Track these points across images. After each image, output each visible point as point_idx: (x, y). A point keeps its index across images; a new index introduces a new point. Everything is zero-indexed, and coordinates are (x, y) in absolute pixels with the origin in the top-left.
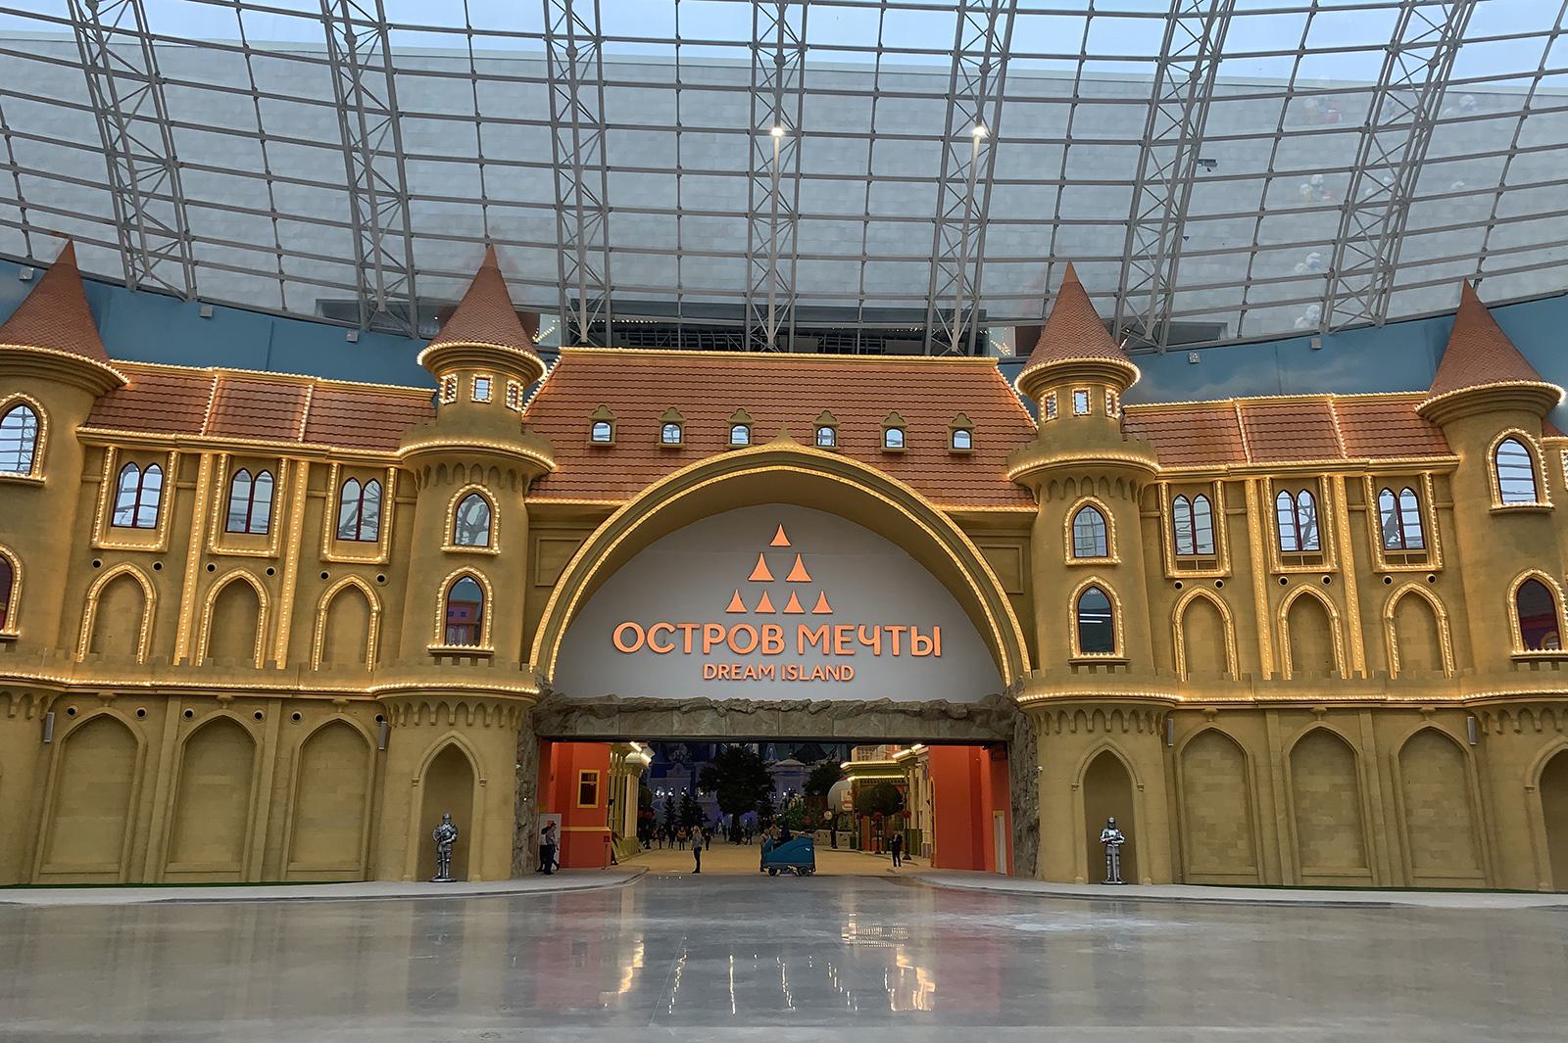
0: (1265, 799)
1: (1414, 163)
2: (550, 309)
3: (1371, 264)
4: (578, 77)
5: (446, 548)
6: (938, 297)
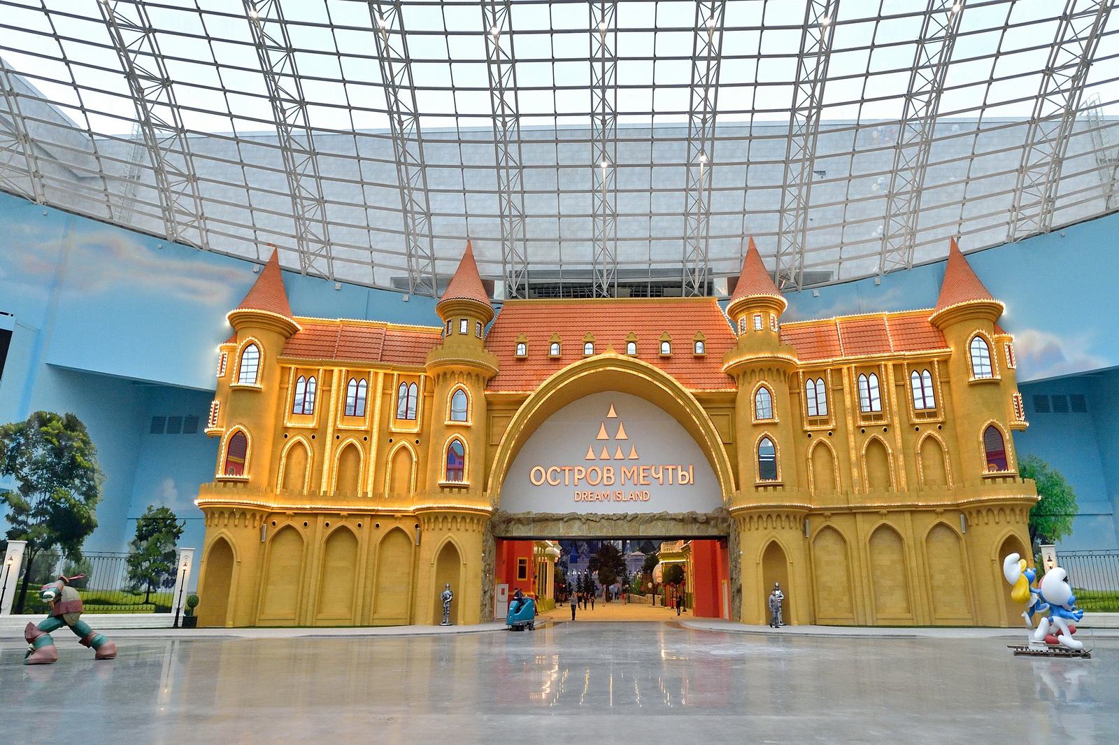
0: (857, 571)
2: (500, 278)
3: (903, 231)
4: (508, 139)
5: (446, 423)
6: (687, 261)
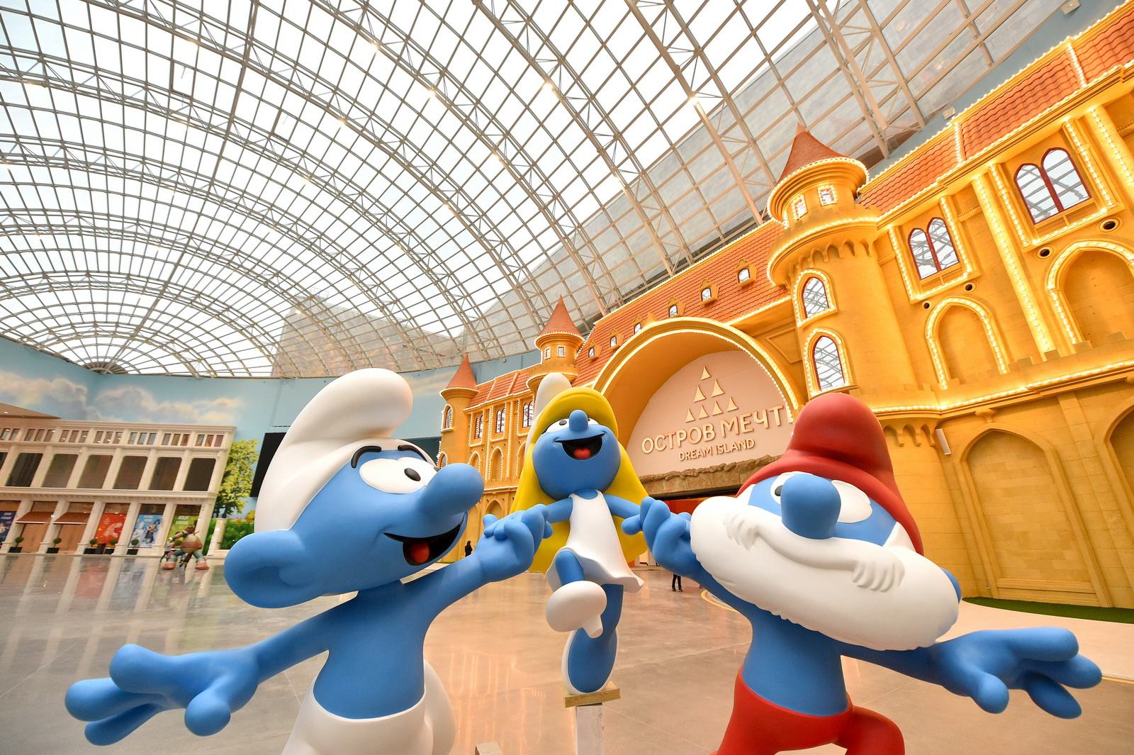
1: (67, 231)
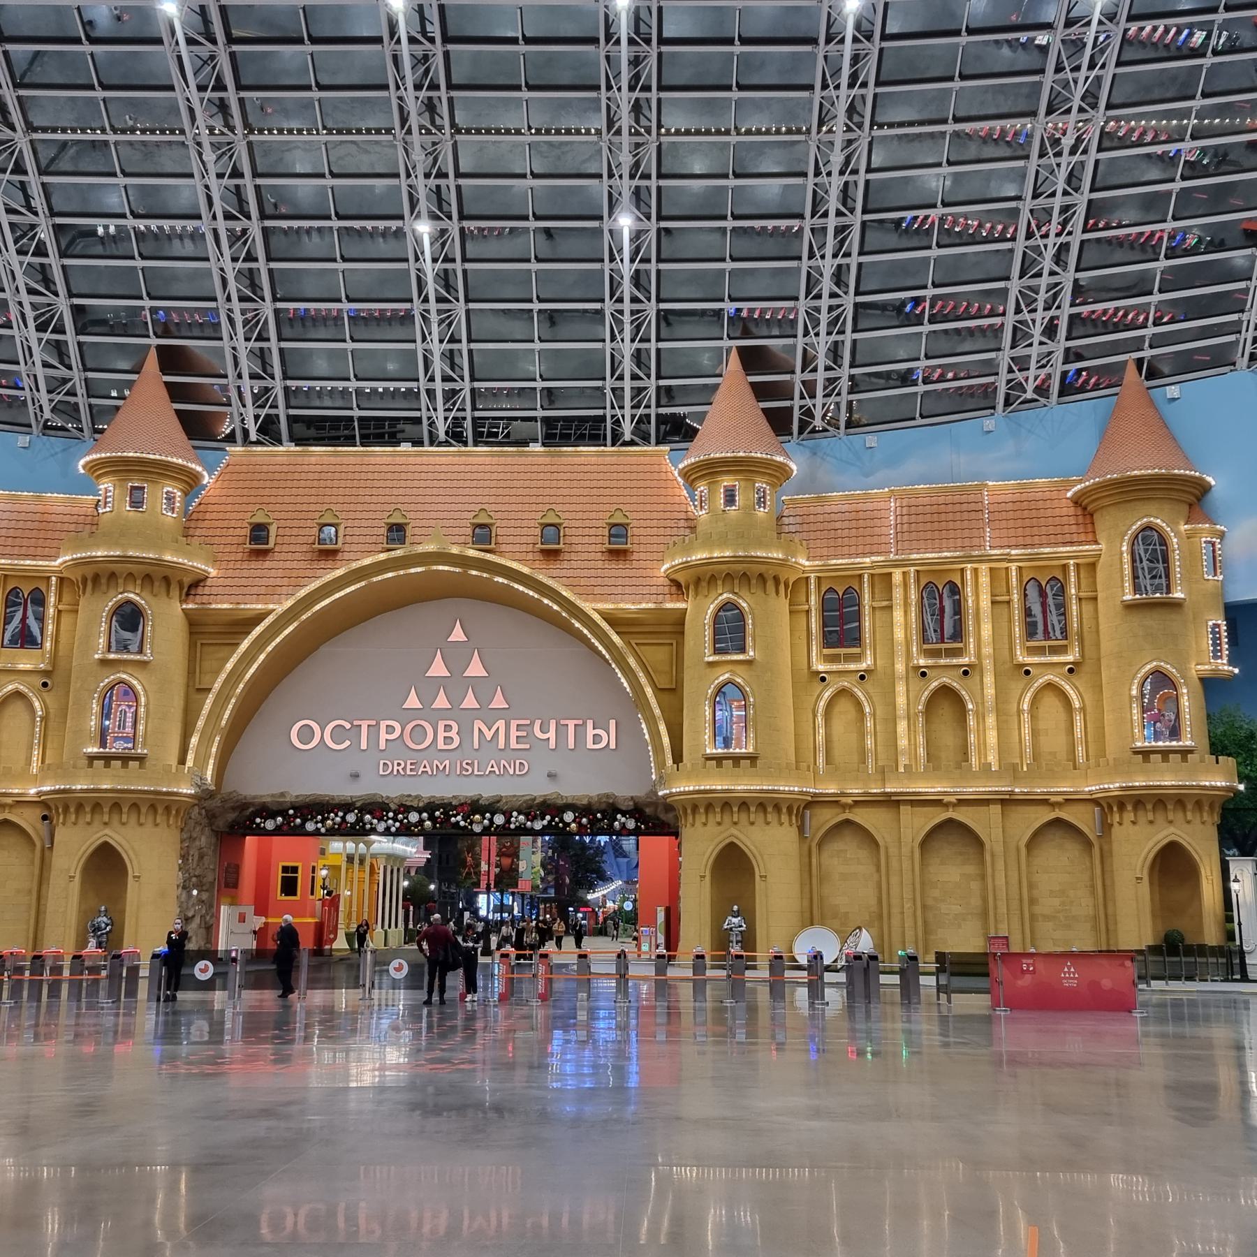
0: (895, 891)
